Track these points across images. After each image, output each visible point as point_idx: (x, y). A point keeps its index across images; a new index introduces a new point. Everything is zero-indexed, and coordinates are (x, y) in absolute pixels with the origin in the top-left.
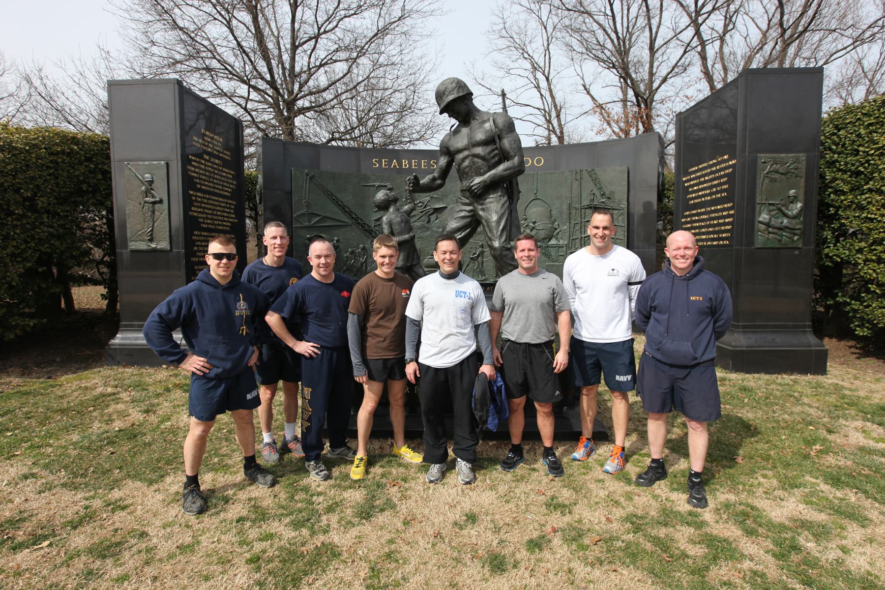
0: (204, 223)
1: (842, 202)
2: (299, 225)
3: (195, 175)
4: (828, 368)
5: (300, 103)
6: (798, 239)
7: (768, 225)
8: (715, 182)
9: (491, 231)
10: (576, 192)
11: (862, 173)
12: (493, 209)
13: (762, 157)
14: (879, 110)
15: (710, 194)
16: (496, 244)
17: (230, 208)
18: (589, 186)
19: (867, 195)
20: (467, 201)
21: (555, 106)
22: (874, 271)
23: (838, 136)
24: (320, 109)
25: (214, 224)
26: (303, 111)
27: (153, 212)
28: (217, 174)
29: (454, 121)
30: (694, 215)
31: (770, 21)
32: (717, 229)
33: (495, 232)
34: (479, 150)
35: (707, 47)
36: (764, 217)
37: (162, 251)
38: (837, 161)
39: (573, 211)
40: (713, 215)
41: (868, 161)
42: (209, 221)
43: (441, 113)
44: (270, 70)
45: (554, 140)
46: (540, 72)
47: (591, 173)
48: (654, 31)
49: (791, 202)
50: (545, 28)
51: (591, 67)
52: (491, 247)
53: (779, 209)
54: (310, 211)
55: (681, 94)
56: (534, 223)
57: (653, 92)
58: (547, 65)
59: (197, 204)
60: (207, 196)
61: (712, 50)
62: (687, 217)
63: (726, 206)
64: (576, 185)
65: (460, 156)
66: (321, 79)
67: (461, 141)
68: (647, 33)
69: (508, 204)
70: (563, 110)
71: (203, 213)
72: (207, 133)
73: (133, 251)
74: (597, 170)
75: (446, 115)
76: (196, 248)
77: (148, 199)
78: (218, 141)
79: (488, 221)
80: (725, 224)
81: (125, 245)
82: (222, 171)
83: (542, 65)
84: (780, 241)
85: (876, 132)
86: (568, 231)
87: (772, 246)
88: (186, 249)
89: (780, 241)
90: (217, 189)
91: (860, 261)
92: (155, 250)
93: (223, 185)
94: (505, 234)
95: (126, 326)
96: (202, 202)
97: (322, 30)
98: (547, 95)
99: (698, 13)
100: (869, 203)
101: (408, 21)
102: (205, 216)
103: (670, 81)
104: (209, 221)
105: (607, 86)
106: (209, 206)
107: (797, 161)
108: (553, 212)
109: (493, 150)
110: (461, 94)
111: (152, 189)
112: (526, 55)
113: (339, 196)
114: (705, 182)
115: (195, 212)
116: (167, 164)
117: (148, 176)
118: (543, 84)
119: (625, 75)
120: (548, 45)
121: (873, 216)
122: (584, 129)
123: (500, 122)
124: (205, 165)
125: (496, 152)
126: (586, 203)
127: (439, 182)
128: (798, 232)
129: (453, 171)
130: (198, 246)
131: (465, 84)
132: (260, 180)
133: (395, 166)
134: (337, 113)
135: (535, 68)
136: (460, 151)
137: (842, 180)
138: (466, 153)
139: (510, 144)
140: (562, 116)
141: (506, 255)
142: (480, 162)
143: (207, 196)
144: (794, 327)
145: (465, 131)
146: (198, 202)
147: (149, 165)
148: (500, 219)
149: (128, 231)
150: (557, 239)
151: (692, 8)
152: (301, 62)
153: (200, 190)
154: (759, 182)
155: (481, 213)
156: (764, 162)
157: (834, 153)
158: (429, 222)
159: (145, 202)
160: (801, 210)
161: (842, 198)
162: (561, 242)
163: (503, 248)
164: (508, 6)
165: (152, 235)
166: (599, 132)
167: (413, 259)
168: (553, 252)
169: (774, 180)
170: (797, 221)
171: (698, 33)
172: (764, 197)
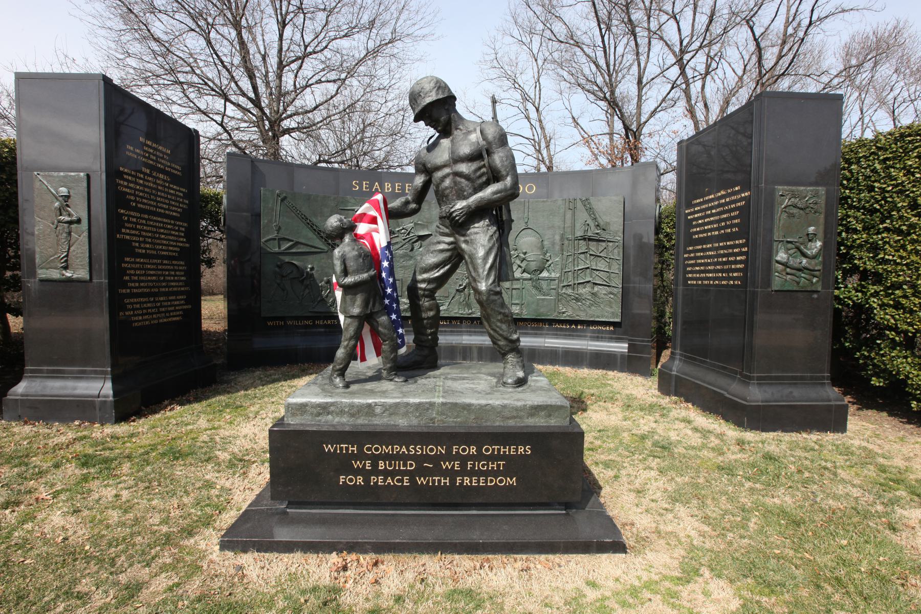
0: (140, 248)
1: (854, 241)
3: (128, 190)
4: (849, 426)
5: (286, 124)
6: (817, 282)
7: (785, 265)
8: (725, 216)
9: (475, 269)
10: (568, 223)
11: (878, 210)
12: (480, 239)
13: (780, 189)
14: (896, 144)
15: (718, 229)
16: (483, 287)
17: (178, 231)
18: (582, 216)
19: (884, 235)
20: (447, 231)
21: (545, 137)
22: (893, 317)
23: (850, 171)
24: (308, 130)
25: (155, 249)
26: (288, 131)
27: (69, 233)
29: (432, 131)
30: (699, 251)
31: (745, 66)
32: (726, 267)
33: (481, 271)
34: (464, 168)
35: (692, 86)
36: (782, 256)
37: (78, 281)
38: (849, 197)
39: (566, 242)
40: (722, 252)
41: (884, 198)
42: (148, 246)
43: (416, 120)
44: (255, 88)
45: (543, 169)
46: (530, 102)
47: (586, 202)
48: (642, 65)
49: (810, 241)
50: (536, 60)
51: (579, 100)
52: (477, 291)
53: (798, 248)
54: (281, 236)
55: (667, 130)
56: (525, 254)
57: (640, 126)
58: (537, 97)
59: (131, 225)
60: (146, 216)
61: (696, 87)
62: (690, 252)
63: (737, 242)
64: (569, 214)
65: (439, 174)
66: (308, 99)
67: (442, 154)
68: (635, 68)
69: (497, 235)
70: (552, 141)
71: (139, 236)
72: (149, 143)
73: (42, 281)
74: (592, 200)
75: (422, 123)
76: (127, 278)
77: (62, 218)
78: (164, 153)
79: (472, 257)
80: (736, 262)
81: (33, 273)
82: (169, 188)
83: (532, 96)
84: (798, 283)
85: (894, 168)
87: (790, 288)
89: (798, 283)
91: (875, 305)
92: (70, 281)
94: (493, 273)
95: (32, 371)
97: (309, 49)
98: (537, 125)
99: (683, 52)
100: (885, 243)
101: (398, 44)
103: (657, 116)
104: (148, 246)
105: (594, 117)
106: (149, 228)
107: (816, 195)
108: (546, 243)
109: (480, 168)
110: (440, 96)
111: (68, 206)
112: (517, 86)
113: (314, 220)
114: (712, 215)
115: (126, 234)
116: (88, 176)
117: (63, 191)
118: (533, 114)
119: (614, 105)
120: (539, 77)
121: (891, 257)
122: (572, 158)
123: (491, 132)
124: (144, 179)
125: (484, 170)
126: (579, 233)
127: (413, 206)
128: (817, 273)
129: (431, 195)
130: (130, 275)
131: (446, 85)
132: (225, 200)
134: (324, 133)
135: (525, 98)
136: (438, 168)
137: (856, 218)
138: (447, 170)
139: (502, 161)
140: (552, 147)
141: (494, 301)
143: (146, 216)
144: (812, 378)
145: (445, 143)
147: (64, 177)
148: (487, 254)
149: (37, 256)
150: (548, 271)
151: (677, 49)
152: (288, 80)
153: (136, 209)
154: (777, 217)
155: (464, 246)
156: (782, 195)
157: (846, 188)
158: (412, 250)
159: (59, 222)
161: (855, 237)
162: (553, 275)
163: (490, 292)
164: (500, 37)
165: (66, 261)
166: (589, 163)
168: (544, 284)
169: (791, 216)
171: (683, 72)
172: (781, 234)
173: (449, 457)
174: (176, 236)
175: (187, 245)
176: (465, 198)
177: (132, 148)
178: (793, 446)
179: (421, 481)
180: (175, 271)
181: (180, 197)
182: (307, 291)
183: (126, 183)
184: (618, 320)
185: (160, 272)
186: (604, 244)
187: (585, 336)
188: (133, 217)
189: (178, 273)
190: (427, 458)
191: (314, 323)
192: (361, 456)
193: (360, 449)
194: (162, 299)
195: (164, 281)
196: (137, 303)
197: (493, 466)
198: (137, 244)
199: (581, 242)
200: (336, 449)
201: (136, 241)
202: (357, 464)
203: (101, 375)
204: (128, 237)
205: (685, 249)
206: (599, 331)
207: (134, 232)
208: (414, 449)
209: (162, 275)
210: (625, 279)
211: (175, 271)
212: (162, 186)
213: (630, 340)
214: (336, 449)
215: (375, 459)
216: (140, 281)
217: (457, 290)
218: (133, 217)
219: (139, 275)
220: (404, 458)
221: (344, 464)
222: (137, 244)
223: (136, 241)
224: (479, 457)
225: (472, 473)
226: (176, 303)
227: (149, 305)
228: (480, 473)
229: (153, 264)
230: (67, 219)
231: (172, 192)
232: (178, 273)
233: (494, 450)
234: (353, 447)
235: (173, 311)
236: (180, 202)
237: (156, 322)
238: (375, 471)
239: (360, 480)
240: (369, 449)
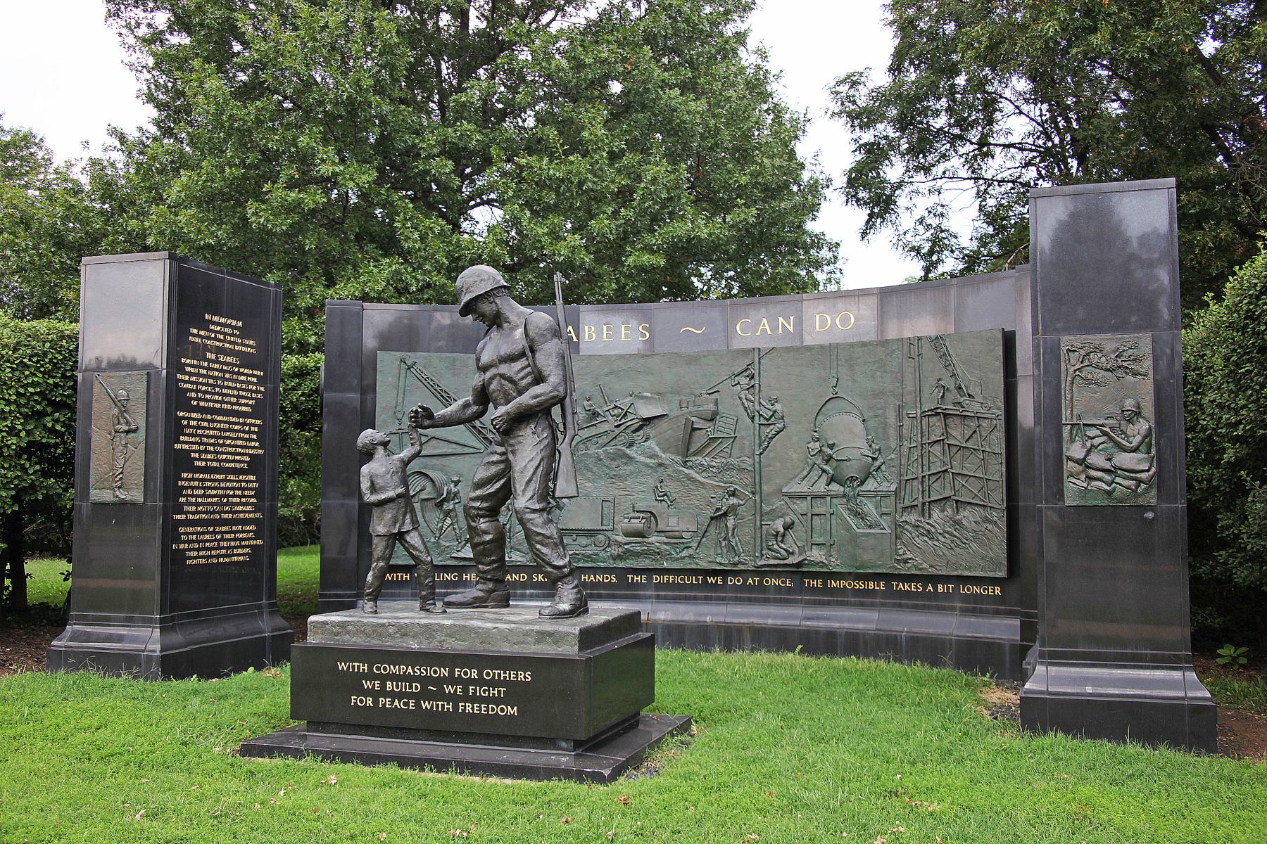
0: (200, 459)
3: (189, 386)
10: (909, 386)
17: (249, 432)
18: (934, 370)
25: (218, 460)
28: (228, 380)
39: (907, 422)
42: (209, 456)
60: (209, 417)
71: (199, 444)
76: (183, 500)
81: (85, 493)
86: (896, 463)
88: (164, 501)
89: (1109, 493)
90: (227, 403)
92: (123, 503)
95: (78, 618)
96: (198, 427)
102: (202, 448)
104: (209, 456)
106: (211, 433)
128: (1144, 476)
130: (188, 496)
143: (209, 417)
146: (193, 427)
162: (884, 487)
168: (869, 507)
170: (1140, 456)
173: (452, 680)
174: (246, 440)
175: (260, 452)
177: (195, 331)
179: (426, 705)
180: (243, 489)
181: (253, 383)
182: (449, 521)
183: (187, 378)
184: (1002, 573)
185: (222, 492)
186: (973, 424)
187: (953, 609)
188: (194, 419)
189: (246, 493)
191: (460, 577)
192: (370, 676)
194: (224, 529)
195: (227, 504)
196: (193, 533)
197: (494, 692)
198: (197, 455)
199: (934, 419)
201: (195, 451)
202: (367, 685)
204: (186, 447)
206: (976, 598)
207: (193, 439)
209: (225, 496)
211: (243, 489)
212: (229, 372)
215: (384, 679)
216: (197, 505)
217: (712, 518)
218: (194, 419)
219: (197, 496)
221: (354, 683)
222: (197, 455)
223: (195, 451)
224: (480, 682)
225: (474, 699)
226: (241, 536)
227: (207, 537)
228: (482, 700)
229: (215, 481)
231: (242, 378)
232: (246, 493)
235: (237, 547)
236: (252, 391)
237: (215, 561)
238: (383, 692)
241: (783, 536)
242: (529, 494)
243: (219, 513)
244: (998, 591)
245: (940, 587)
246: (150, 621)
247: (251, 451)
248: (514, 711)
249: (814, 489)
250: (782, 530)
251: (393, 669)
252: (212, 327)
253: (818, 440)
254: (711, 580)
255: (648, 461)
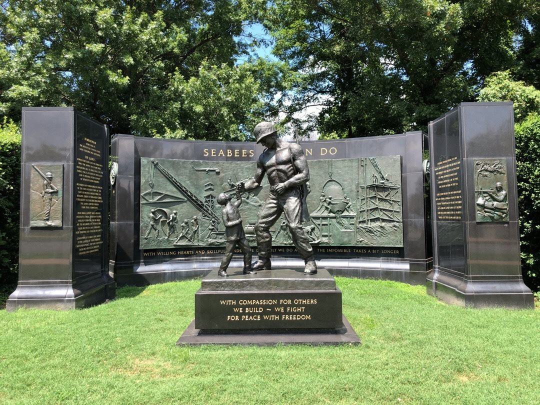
2: (145, 202)
15: (450, 183)
27: (51, 199)
29: (265, 147)
33: (292, 217)
36: (480, 201)
77: (48, 190)
81: (27, 223)
93: (95, 176)
95: (22, 283)
133: (221, 155)
138: (274, 168)
142: (282, 175)
144: (62, 283)
146: (81, 190)
156: (477, 164)
160: (506, 196)
165: (49, 216)
167: (241, 235)
170: (504, 203)
173: (278, 305)
176: (284, 182)
178: (145, 176)
179: (266, 317)
190: (268, 306)
192: (238, 306)
193: (237, 302)
200: (226, 303)
202: (236, 310)
203: (63, 284)
205: (436, 195)
208: (262, 301)
210: (404, 216)
213: (411, 261)
214: (226, 303)
215: (244, 307)
220: (258, 306)
221: (230, 310)
224: (292, 305)
225: (289, 313)
228: (293, 313)
230: (51, 191)
233: (299, 301)
234: (234, 301)
239: (237, 318)
240: (241, 302)
241: (311, 233)
242: (297, 221)
243: (90, 230)
244: (398, 252)
245: (374, 251)
246: (67, 283)
247: (99, 201)
248: (309, 317)
249: (323, 215)
250: (228, 204)
251: (250, 302)
252: (87, 144)
253: (324, 196)
254: (280, 250)
255: (255, 204)
